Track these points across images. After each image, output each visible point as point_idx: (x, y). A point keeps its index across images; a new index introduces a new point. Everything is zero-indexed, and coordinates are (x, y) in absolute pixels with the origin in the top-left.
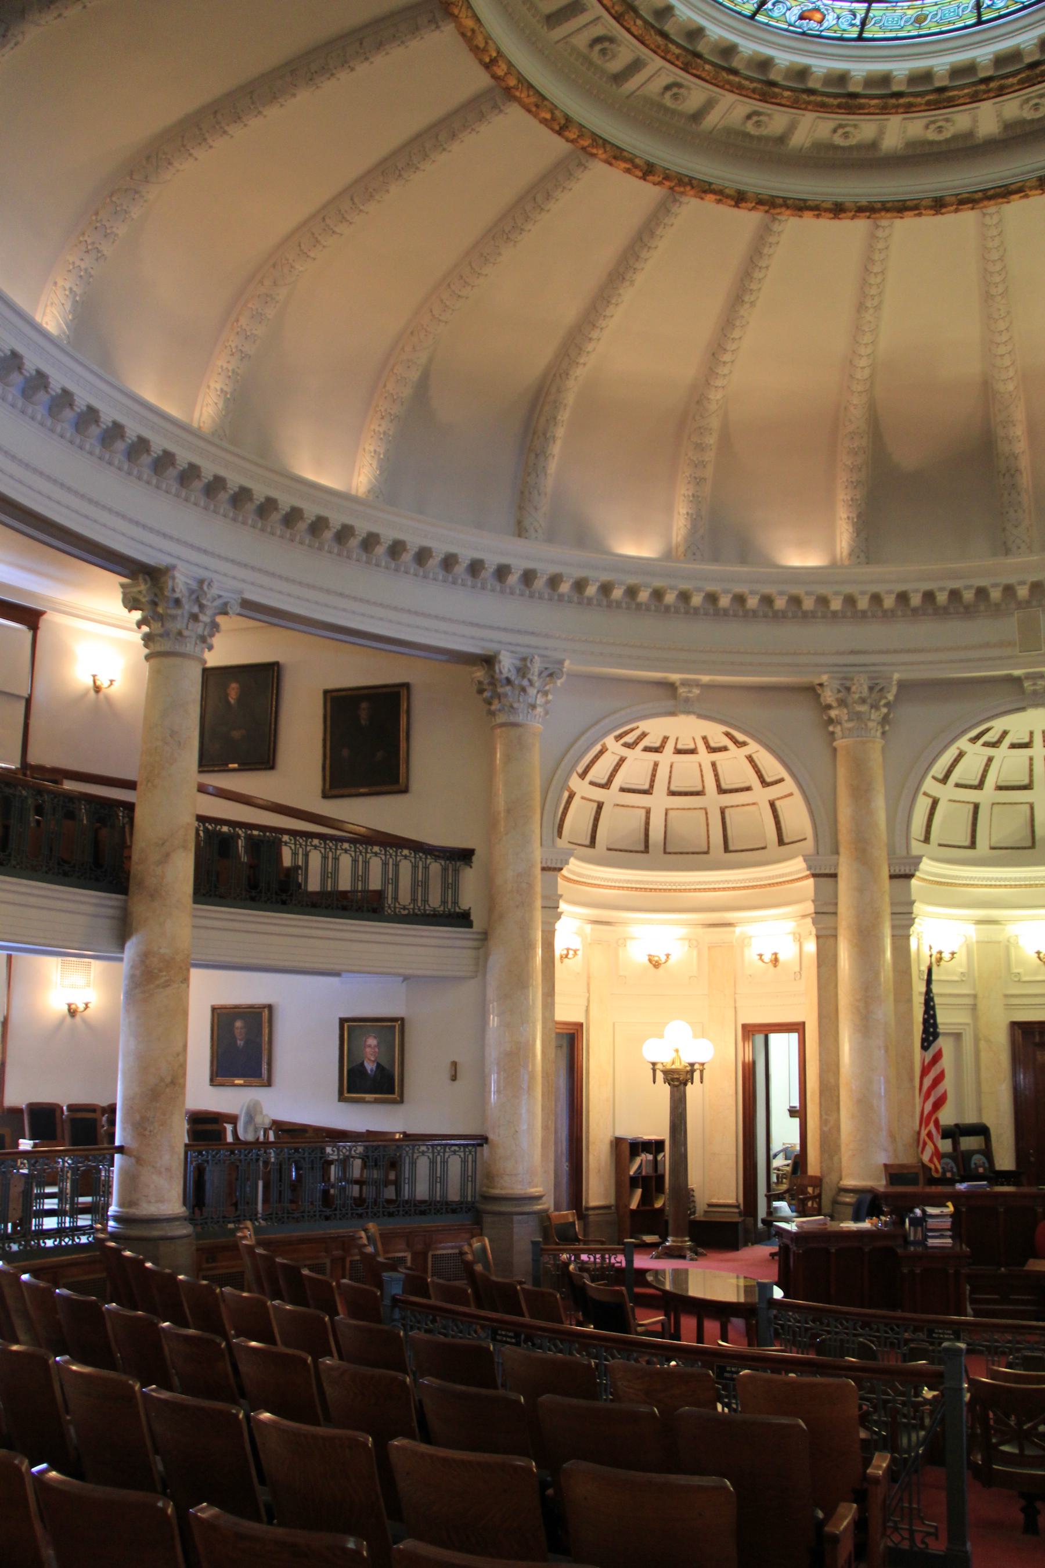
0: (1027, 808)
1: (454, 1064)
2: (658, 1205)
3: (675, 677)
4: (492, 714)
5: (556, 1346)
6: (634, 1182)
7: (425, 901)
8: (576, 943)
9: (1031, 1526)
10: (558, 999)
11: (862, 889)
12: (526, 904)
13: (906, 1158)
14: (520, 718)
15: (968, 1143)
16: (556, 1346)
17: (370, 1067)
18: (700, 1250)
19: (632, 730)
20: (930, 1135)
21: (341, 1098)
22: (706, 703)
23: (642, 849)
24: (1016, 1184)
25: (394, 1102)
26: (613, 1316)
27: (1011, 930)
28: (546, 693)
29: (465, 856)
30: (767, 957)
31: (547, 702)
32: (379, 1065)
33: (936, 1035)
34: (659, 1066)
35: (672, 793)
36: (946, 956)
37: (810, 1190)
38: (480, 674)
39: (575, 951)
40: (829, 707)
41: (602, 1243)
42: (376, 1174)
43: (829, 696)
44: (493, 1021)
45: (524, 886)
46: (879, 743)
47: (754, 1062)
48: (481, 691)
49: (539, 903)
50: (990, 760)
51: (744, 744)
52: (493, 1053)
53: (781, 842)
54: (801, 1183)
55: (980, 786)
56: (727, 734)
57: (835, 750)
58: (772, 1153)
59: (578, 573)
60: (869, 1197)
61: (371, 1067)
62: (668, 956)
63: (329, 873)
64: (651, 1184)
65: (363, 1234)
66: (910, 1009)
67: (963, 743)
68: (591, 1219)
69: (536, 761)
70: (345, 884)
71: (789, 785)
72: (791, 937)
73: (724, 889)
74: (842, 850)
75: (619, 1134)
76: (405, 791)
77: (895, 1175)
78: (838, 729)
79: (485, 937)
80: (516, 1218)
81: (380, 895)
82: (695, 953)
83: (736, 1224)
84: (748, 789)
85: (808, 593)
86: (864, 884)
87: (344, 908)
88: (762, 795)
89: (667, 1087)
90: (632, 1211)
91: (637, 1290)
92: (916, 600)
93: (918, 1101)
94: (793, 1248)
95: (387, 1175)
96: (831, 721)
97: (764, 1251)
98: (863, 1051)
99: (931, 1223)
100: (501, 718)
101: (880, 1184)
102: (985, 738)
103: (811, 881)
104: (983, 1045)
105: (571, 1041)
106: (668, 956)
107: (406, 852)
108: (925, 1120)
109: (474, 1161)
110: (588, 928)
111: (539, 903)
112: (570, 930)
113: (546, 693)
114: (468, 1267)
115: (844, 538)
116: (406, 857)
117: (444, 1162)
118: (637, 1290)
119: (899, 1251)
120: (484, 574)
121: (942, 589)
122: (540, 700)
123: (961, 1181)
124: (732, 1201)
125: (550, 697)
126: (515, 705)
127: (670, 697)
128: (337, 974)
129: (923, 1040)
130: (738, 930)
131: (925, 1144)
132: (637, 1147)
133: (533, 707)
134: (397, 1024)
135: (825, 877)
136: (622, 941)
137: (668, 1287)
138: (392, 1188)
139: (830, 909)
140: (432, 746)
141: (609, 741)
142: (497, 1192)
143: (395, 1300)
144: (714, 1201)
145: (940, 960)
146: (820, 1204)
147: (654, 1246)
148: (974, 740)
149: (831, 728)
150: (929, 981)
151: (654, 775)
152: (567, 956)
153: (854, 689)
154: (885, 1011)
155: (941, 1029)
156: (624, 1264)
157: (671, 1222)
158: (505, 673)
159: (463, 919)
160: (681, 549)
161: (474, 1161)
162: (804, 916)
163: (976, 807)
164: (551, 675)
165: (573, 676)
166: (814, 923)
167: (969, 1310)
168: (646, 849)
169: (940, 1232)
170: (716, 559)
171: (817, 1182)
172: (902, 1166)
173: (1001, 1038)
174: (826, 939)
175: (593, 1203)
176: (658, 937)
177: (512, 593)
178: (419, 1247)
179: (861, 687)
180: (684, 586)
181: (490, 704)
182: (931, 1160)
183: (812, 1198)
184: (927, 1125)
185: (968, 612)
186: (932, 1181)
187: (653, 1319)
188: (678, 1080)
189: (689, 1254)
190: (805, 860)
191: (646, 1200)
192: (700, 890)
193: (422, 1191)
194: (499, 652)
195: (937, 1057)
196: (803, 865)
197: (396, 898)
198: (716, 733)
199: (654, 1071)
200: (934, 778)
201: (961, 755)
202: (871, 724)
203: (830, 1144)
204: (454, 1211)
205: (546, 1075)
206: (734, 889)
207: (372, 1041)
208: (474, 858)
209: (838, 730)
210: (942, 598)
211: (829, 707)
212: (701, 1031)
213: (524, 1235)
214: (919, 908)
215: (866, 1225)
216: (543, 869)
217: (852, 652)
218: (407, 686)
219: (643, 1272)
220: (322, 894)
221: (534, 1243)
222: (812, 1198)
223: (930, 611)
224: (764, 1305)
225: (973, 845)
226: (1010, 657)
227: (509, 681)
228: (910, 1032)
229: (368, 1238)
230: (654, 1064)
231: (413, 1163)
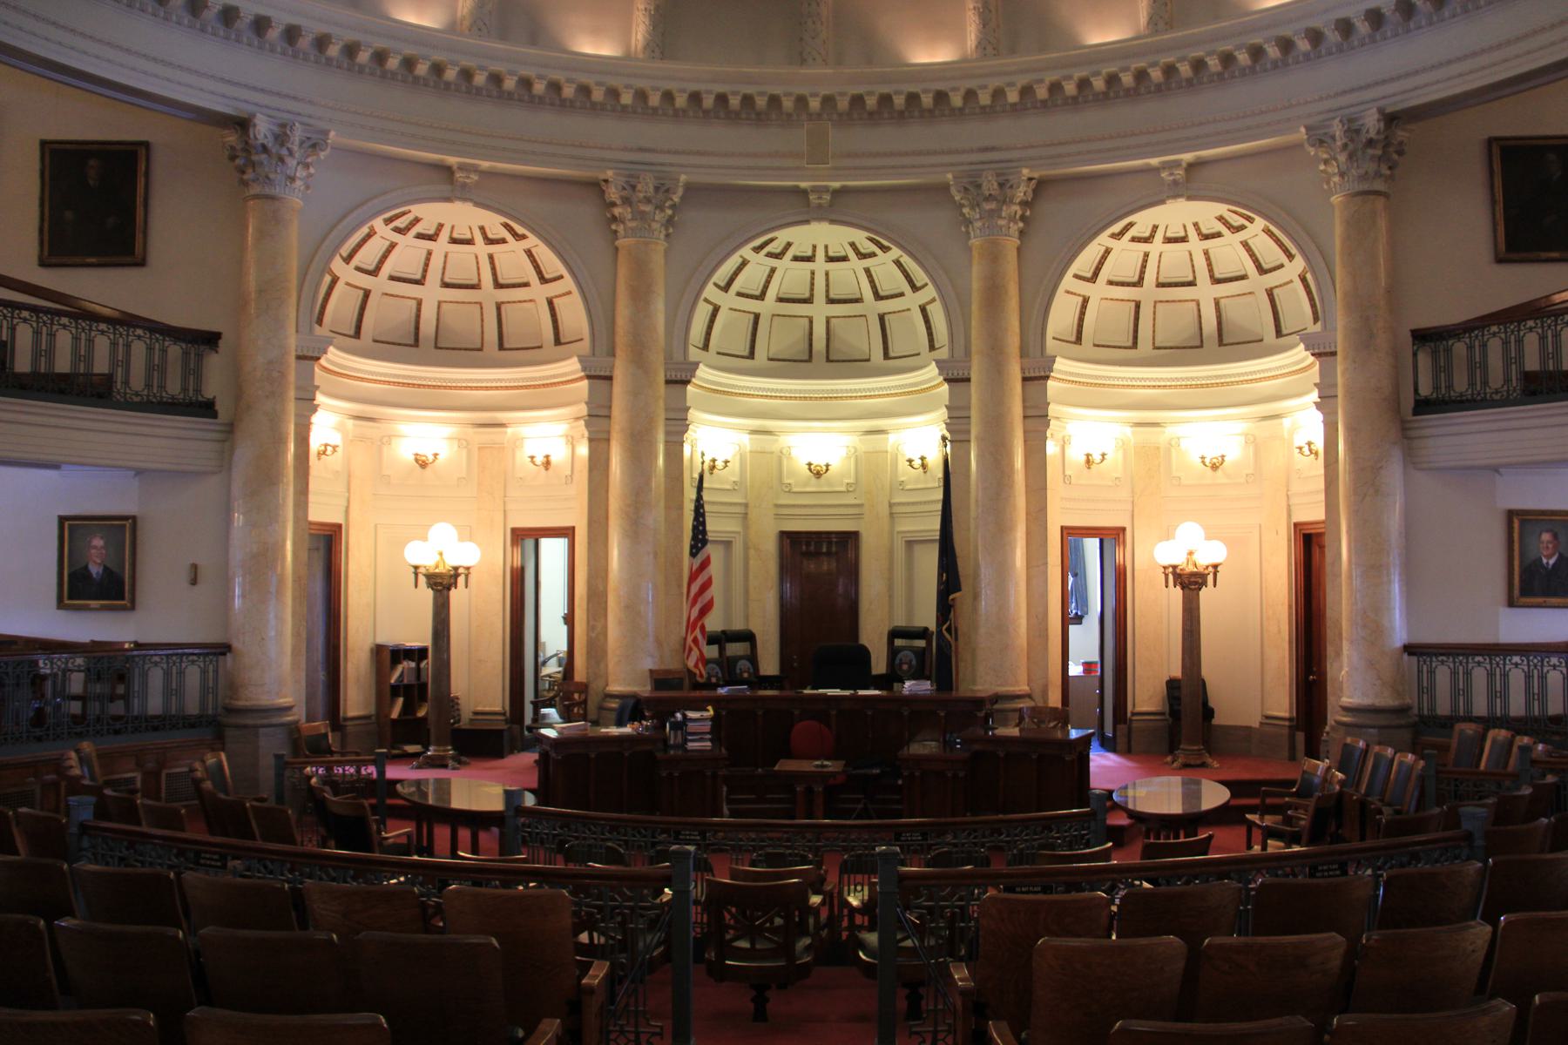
0: (806, 321)
1: (195, 567)
2: (421, 713)
3: (452, 160)
4: (245, 184)
5: (265, 867)
6: (396, 690)
7: (162, 387)
8: (336, 439)
9: (760, 1014)
10: (312, 498)
11: (637, 393)
12: (277, 394)
13: (672, 664)
14: (276, 191)
15: (735, 649)
16: (265, 867)
17: (95, 570)
18: (464, 759)
19: (404, 214)
20: (695, 641)
21: (61, 604)
22: (485, 190)
23: (411, 342)
24: (781, 688)
25: (123, 608)
26: (353, 831)
27: (785, 441)
28: (307, 166)
29: (211, 339)
30: (539, 460)
31: (310, 175)
32: (106, 569)
33: (705, 542)
34: (422, 570)
35: (446, 285)
36: (719, 464)
37: (576, 696)
38: (232, 138)
39: (335, 448)
40: (614, 204)
41: (357, 754)
42: (98, 688)
43: (613, 194)
44: (238, 519)
45: (275, 374)
46: (661, 246)
47: (522, 569)
48: (233, 158)
49: (292, 394)
50: (773, 270)
51: (524, 237)
52: (237, 555)
53: (558, 342)
54: (569, 693)
55: (761, 297)
56: (506, 226)
57: (617, 249)
58: (541, 659)
59: (351, 36)
60: (631, 702)
61: (97, 567)
62: (436, 455)
63: (44, 351)
64: (413, 692)
65: (73, 755)
66: (681, 516)
67: (746, 252)
68: (1134, 725)
69: (294, 239)
70: (63, 365)
71: (568, 283)
72: (563, 440)
73: (497, 388)
74: (619, 352)
75: (381, 640)
76: (141, 263)
77: (661, 680)
78: (621, 228)
79: (230, 429)
80: (261, 730)
81: (109, 379)
82: (464, 453)
83: (501, 731)
84: (526, 285)
85: (599, 84)
86: (636, 390)
87: (62, 392)
88: (539, 292)
89: (430, 592)
90: (394, 721)
91: (389, 801)
92: (708, 102)
93: (685, 607)
94: (553, 754)
95: (114, 688)
96: (614, 219)
97: (531, 757)
98: (631, 558)
99: (691, 727)
100: (255, 189)
101: (645, 689)
102: (768, 249)
103: (586, 382)
104: (752, 552)
105: (327, 544)
106: (436, 455)
107: (139, 332)
108: (691, 626)
109: (216, 671)
110: (350, 423)
111: (292, 394)
112: (328, 425)
113: (307, 166)
114: (197, 783)
115: (640, 33)
116: (139, 337)
117: (181, 673)
118: (389, 801)
119: (659, 755)
120: (238, 24)
121: (735, 93)
122: (301, 173)
123: (722, 686)
124: (498, 709)
125: (312, 170)
126: (272, 176)
127: (446, 182)
128: (55, 466)
129: (692, 547)
130: (509, 430)
131: (691, 650)
132: (399, 654)
133: (292, 179)
134: (128, 524)
135: (600, 378)
136: (389, 438)
137: (431, 801)
138: (121, 703)
139: (603, 412)
140: (175, 215)
141: (378, 223)
142: (241, 703)
143: (84, 828)
144: (480, 708)
145: (713, 468)
146: (585, 710)
147: (416, 755)
148: (757, 249)
149: (614, 227)
150: (700, 488)
151: (427, 265)
152: (324, 452)
153: (639, 187)
154: (656, 516)
155: (710, 536)
156: (375, 776)
157: (433, 731)
158: (261, 139)
159: (206, 409)
160: (467, 23)
161: (216, 671)
162: (578, 419)
163: (757, 317)
164: (314, 146)
165: (338, 149)
166: (587, 425)
167: (726, 811)
168: (416, 343)
169: (700, 736)
170: (503, 37)
171: (584, 688)
172: (668, 672)
173: (770, 547)
174: (599, 443)
175: (351, 714)
176: (424, 435)
177: (272, 50)
178: (150, 765)
179: (647, 186)
180: (466, 62)
181: (243, 172)
182: (696, 666)
183: (578, 704)
184: (694, 630)
185: (760, 119)
186: (696, 686)
187: (397, 832)
188: (442, 584)
189: (451, 763)
190: (581, 361)
191: (408, 708)
192: (471, 388)
193: (155, 704)
194: (254, 116)
195: (706, 563)
196: (578, 366)
197: (126, 383)
198: (494, 223)
199: (416, 574)
200: (716, 285)
201: (744, 263)
202: (655, 226)
203: (597, 649)
204: (192, 726)
205: (297, 580)
206: (507, 388)
207: (98, 542)
208: (221, 342)
209: (621, 228)
210: (735, 102)
211: (614, 204)
212: (467, 534)
213: (270, 746)
214: (693, 414)
215: (627, 730)
216: (299, 358)
217: (641, 150)
218: (146, 145)
219: (395, 782)
220: (35, 375)
221: (278, 757)
222: (578, 704)
223: (722, 115)
224: (511, 813)
225: (751, 355)
226: (798, 168)
227: (265, 149)
228: (680, 538)
229: (81, 760)
230: (416, 568)
231: (144, 675)
